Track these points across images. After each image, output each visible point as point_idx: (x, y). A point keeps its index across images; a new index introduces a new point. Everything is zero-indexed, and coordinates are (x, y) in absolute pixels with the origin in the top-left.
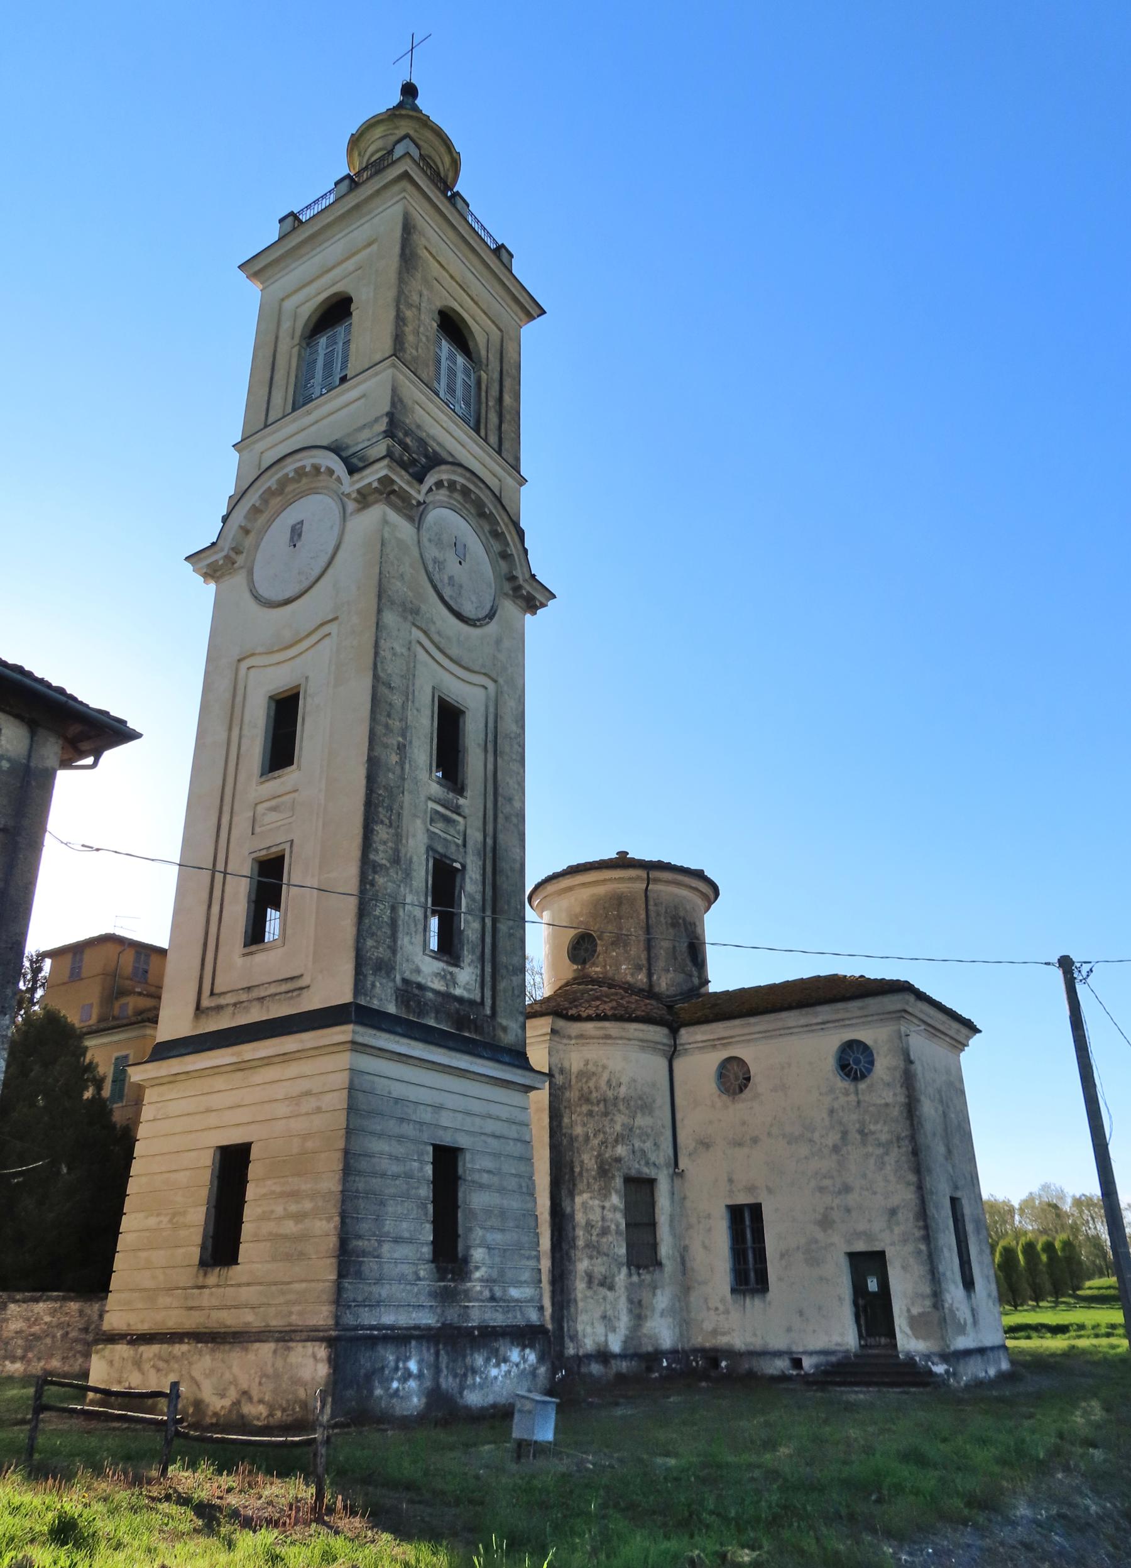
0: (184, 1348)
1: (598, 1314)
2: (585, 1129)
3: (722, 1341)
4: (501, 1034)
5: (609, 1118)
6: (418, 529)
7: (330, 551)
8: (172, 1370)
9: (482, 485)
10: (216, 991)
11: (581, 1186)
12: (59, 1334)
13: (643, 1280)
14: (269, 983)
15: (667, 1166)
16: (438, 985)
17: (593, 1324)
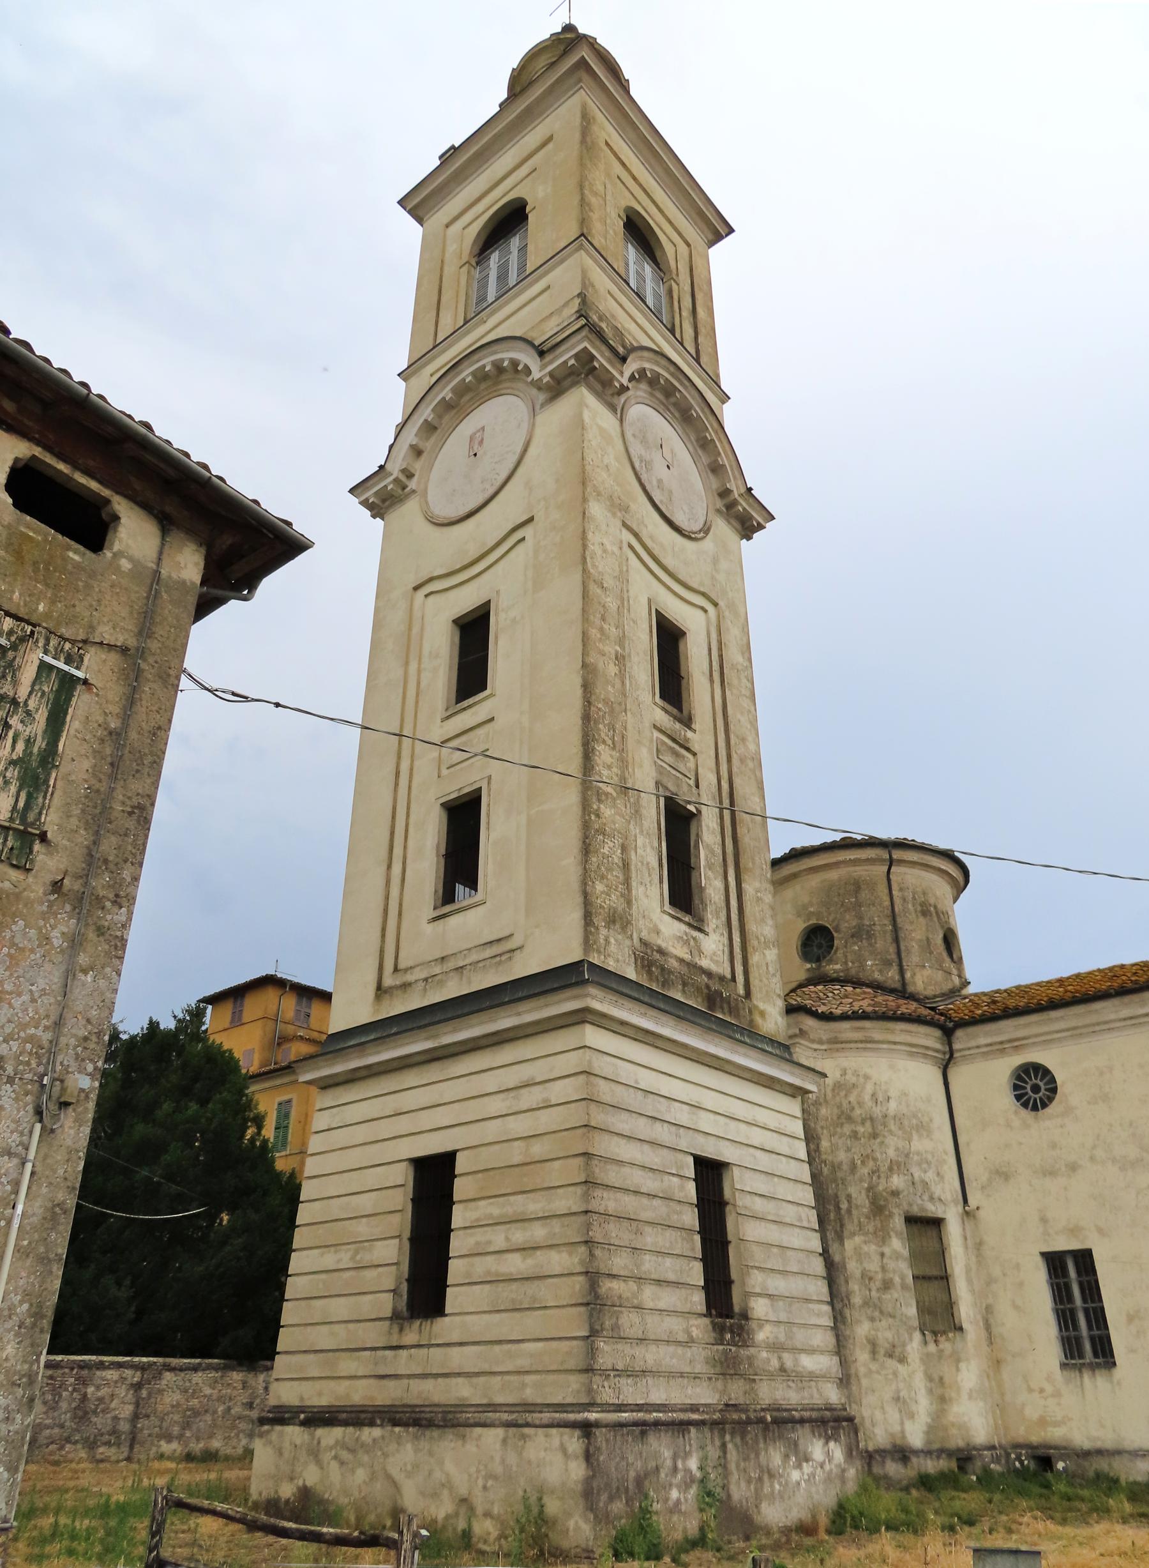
0: (377, 1432)
1: (888, 1395)
2: (849, 1155)
3: (1055, 1434)
4: (758, 1020)
5: (878, 1140)
6: (621, 421)
7: (519, 449)
8: (361, 1465)
9: (686, 382)
10: (401, 966)
11: (850, 1227)
12: (221, 1409)
13: (942, 1351)
14: (469, 949)
15: (955, 1202)
16: (681, 952)
17: (882, 1408)
